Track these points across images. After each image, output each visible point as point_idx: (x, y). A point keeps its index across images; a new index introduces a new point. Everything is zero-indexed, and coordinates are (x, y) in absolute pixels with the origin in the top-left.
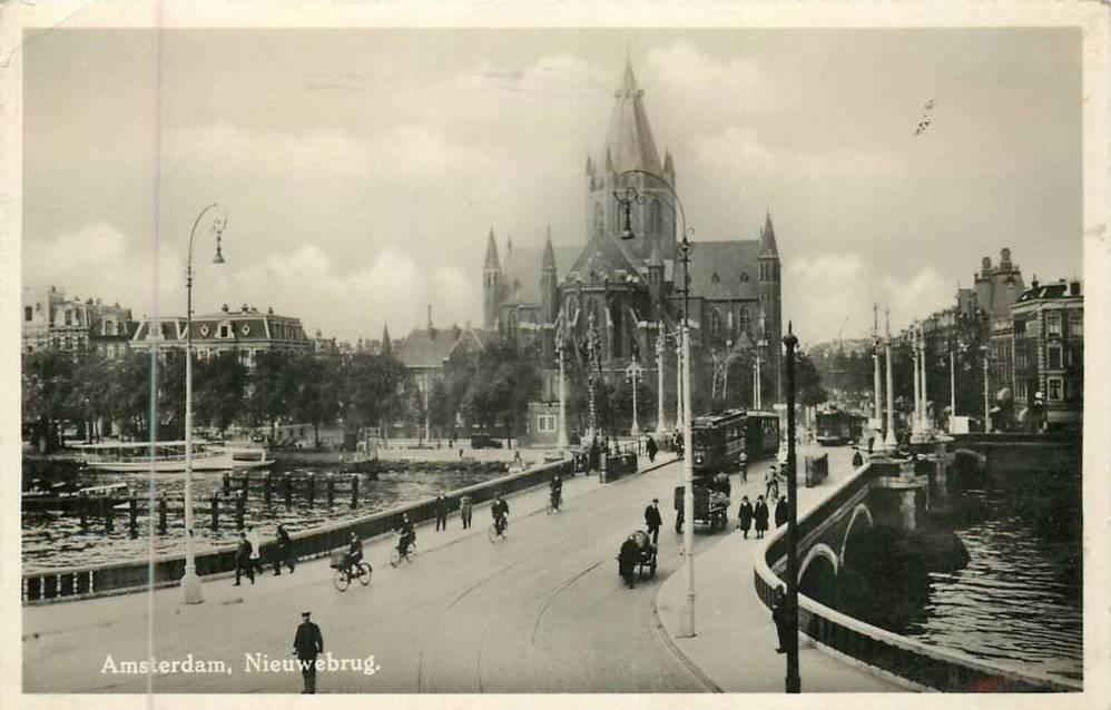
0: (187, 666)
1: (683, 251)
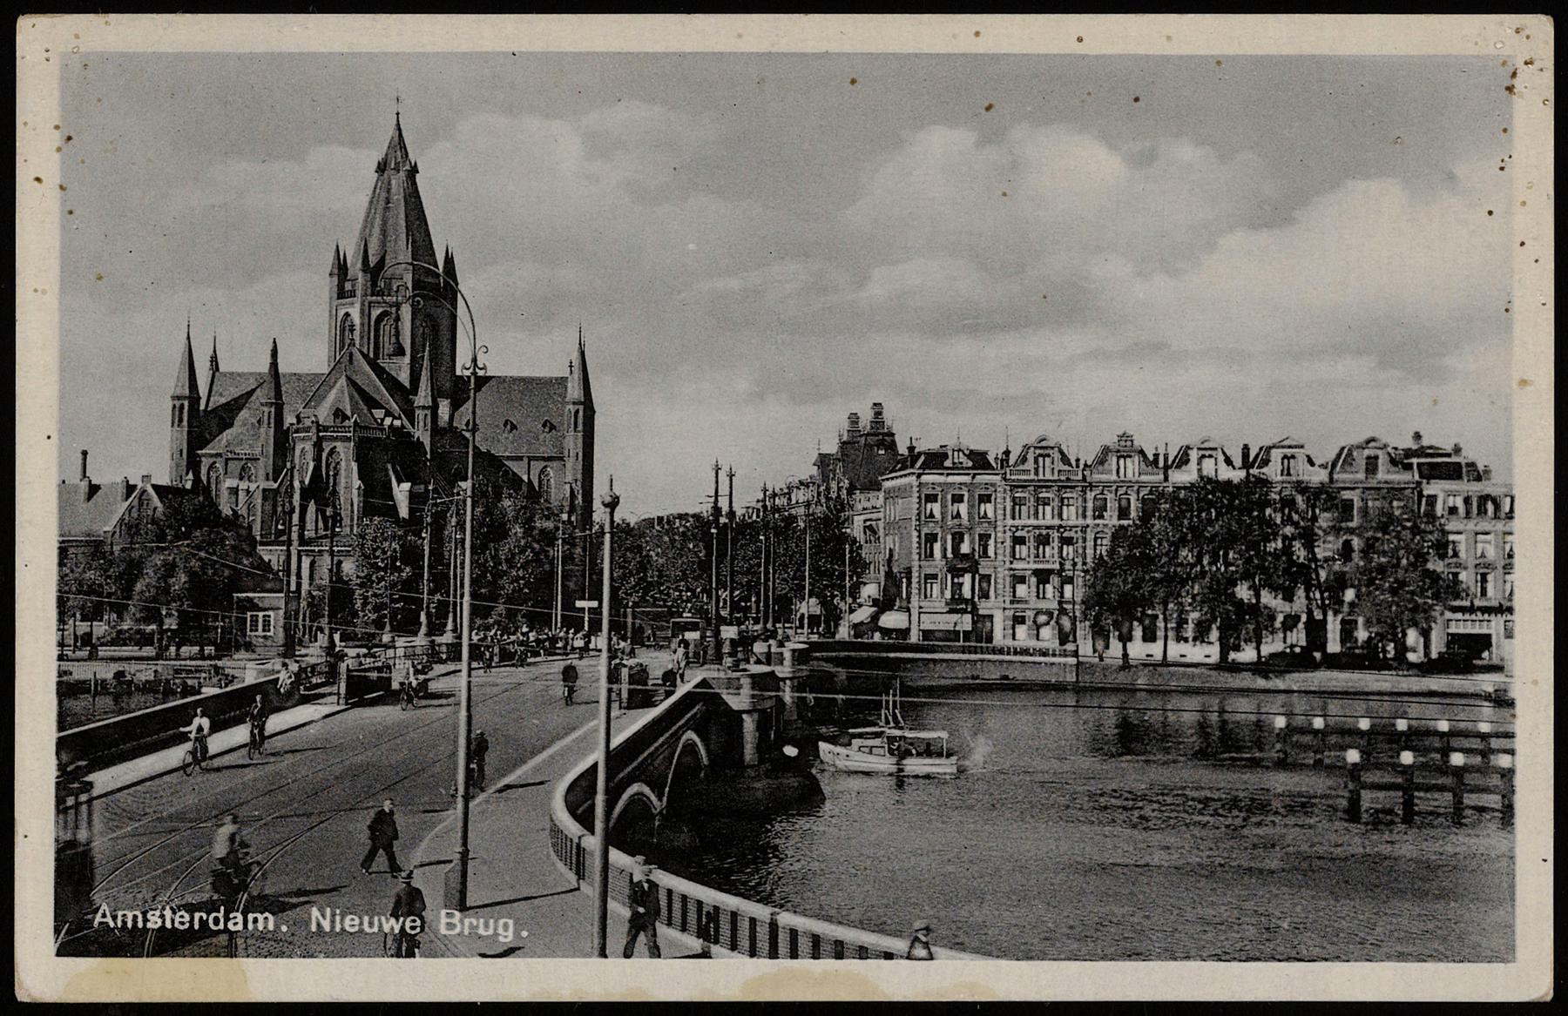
0: (216, 921)
1: (458, 391)
